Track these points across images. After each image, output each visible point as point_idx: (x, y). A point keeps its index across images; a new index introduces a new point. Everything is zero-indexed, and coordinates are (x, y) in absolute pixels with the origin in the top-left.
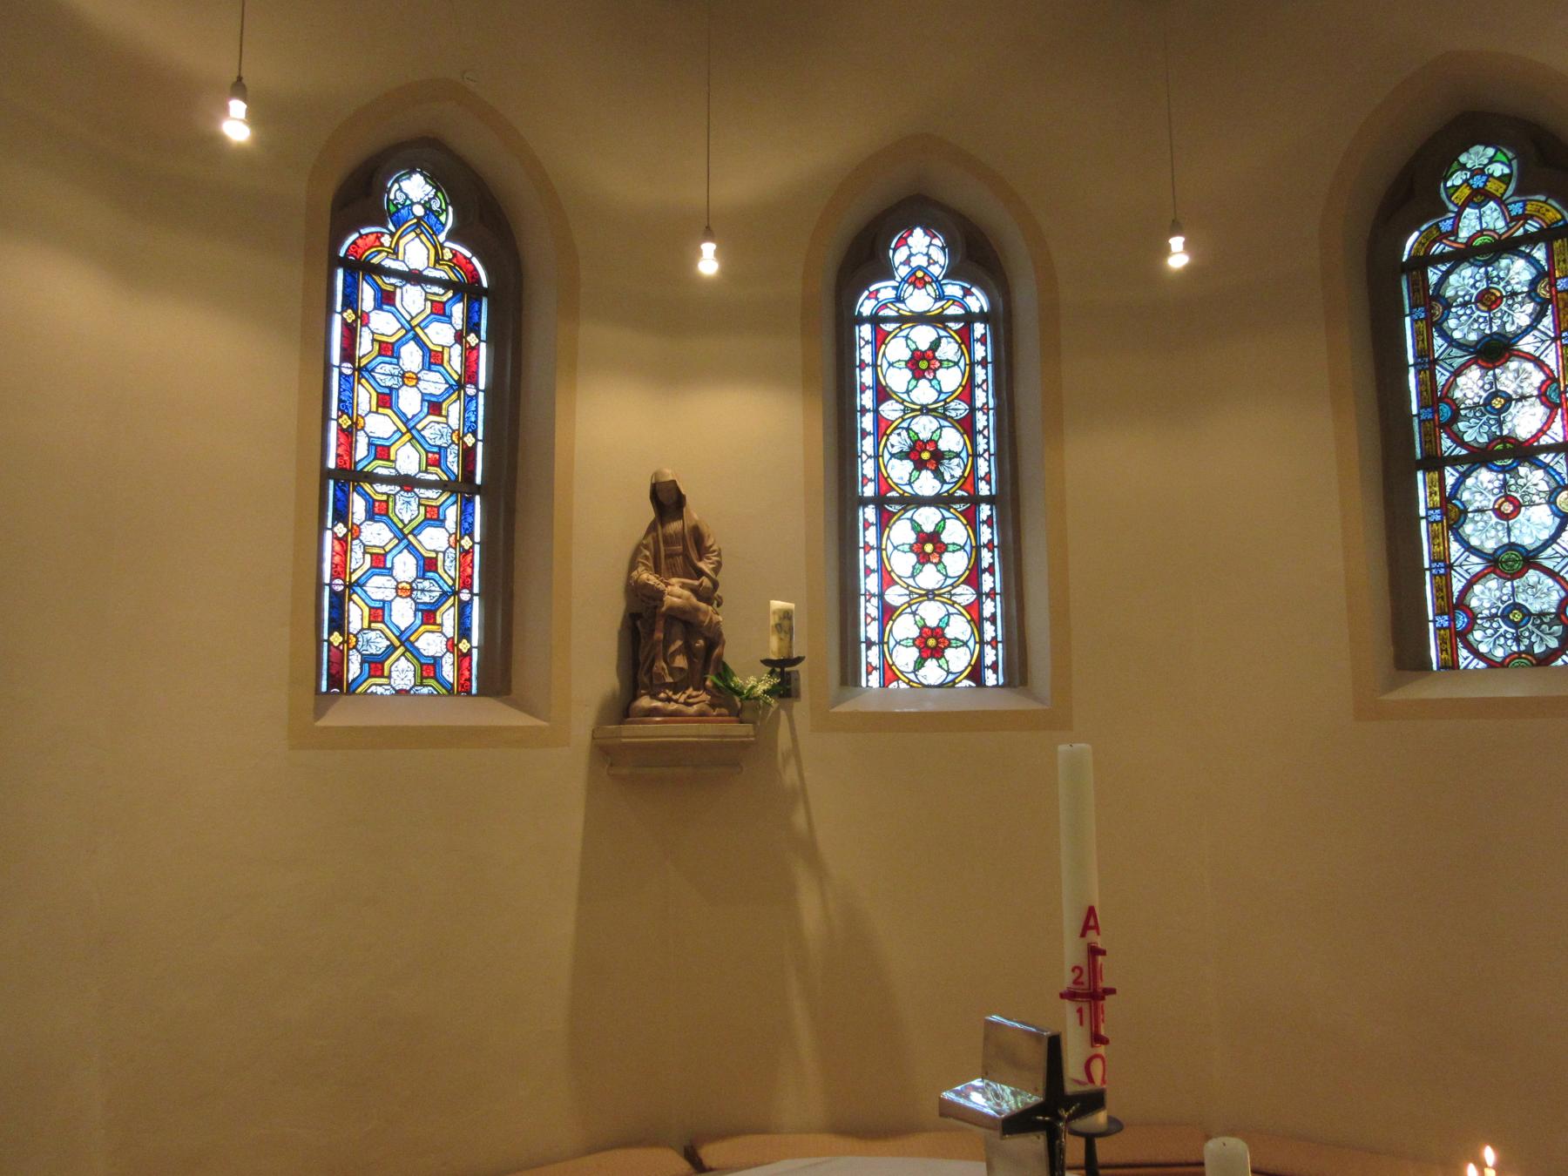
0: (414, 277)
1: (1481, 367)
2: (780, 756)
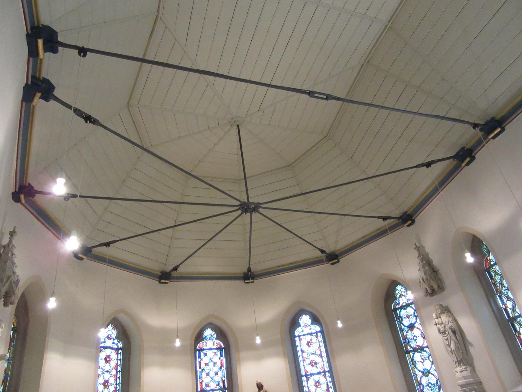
1: (411, 331)
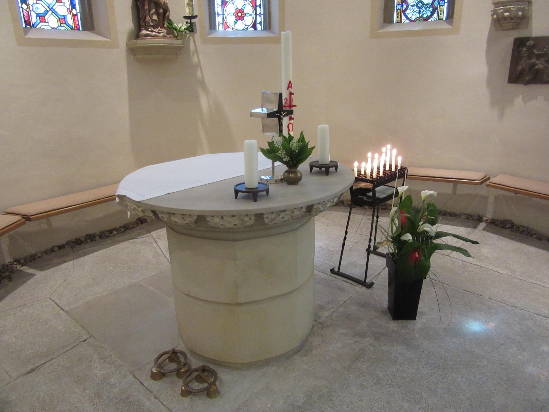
2: (191, 53)
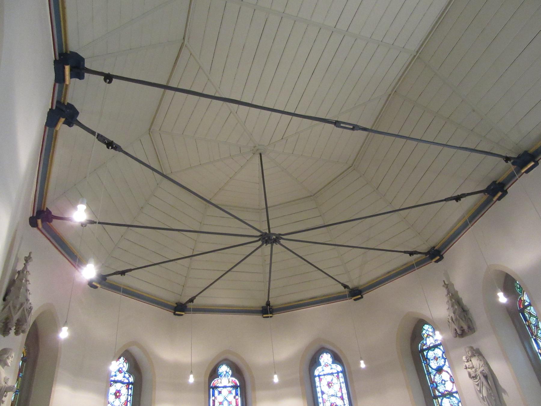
0: (225, 387)
